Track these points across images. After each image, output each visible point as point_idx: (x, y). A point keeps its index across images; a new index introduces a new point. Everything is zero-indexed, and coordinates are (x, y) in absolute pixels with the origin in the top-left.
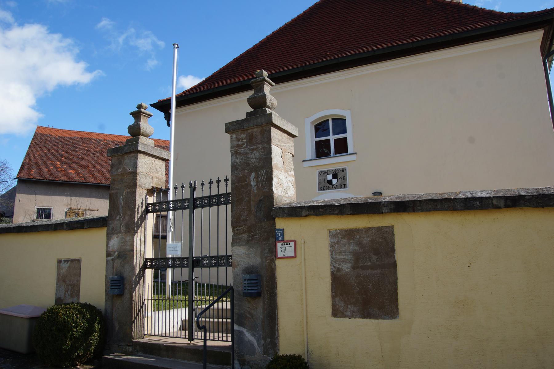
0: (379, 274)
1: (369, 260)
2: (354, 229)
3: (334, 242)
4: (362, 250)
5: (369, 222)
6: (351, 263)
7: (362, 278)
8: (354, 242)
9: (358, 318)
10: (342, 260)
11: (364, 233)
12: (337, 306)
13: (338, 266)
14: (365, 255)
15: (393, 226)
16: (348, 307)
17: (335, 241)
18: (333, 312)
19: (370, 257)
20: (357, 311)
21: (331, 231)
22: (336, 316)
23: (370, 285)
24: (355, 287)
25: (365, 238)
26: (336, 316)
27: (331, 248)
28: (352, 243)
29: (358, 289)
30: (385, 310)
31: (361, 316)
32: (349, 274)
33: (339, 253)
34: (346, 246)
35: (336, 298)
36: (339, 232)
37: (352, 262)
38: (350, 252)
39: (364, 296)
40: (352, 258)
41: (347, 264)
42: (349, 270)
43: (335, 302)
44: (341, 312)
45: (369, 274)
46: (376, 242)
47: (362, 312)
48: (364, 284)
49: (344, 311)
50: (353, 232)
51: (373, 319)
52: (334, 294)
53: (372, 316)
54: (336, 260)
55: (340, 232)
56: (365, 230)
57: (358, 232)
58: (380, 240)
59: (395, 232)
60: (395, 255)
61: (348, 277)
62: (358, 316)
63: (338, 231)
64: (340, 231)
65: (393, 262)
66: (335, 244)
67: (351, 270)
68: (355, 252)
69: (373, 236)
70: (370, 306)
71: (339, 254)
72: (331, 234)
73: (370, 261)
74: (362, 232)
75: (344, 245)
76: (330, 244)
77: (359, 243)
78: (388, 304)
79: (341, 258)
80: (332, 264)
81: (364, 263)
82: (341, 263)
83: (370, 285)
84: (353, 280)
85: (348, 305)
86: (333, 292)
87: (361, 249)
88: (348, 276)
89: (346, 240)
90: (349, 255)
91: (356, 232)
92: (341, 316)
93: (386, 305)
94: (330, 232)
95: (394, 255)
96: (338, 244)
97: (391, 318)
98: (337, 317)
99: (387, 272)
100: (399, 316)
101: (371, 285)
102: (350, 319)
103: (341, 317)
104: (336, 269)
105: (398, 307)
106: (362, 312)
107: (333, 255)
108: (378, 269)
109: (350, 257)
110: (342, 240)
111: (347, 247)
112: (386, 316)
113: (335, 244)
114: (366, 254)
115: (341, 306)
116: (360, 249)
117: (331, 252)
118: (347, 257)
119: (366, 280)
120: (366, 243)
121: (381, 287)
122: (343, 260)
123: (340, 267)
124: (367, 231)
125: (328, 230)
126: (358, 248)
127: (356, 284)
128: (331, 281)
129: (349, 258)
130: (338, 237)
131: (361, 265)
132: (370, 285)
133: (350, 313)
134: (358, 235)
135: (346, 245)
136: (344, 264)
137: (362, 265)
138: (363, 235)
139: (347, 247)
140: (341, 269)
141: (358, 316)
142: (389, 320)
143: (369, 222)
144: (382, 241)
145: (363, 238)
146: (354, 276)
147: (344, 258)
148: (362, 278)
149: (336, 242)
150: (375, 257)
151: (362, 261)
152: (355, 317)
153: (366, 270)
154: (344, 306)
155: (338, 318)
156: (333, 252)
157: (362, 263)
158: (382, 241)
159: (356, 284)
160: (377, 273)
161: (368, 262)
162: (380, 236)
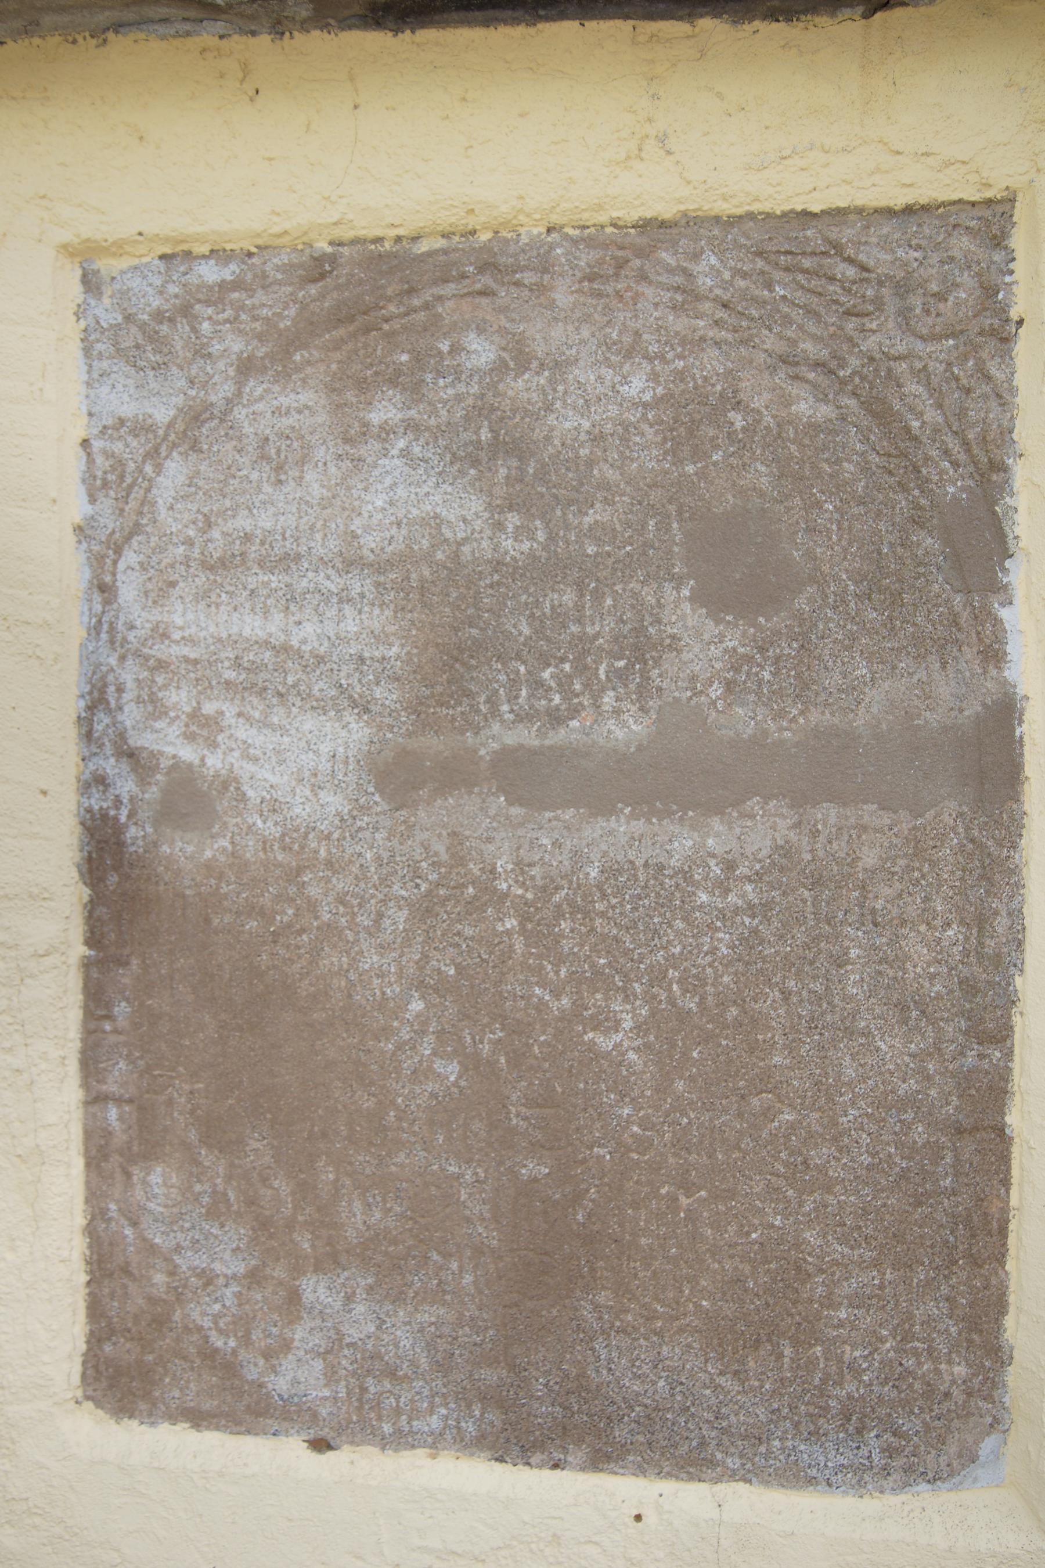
0: (756, 878)
1: (622, 676)
2: (423, 247)
3: (141, 428)
4: (523, 532)
5: (662, 139)
6: (364, 707)
7: (511, 923)
8: (412, 427)
9: (435, 1443)
10: (237, 663)
11: (563, 296)
12: (160, 1278)
13: (188, 753)
14: (569, 598)
15: (1011, 200)
16: (294, 1297)
17: (162, 414)
18: (95, 1340)
19: (639, 630)
20: (424, 1362)
21: (107, 266)
22: (147, 1395)
23: (616, 1027)
24: (405, 1034)
25: (583, 374)
26: (147, 1395)
27: (106, 504)
28: (386, 432)
29: (451, 1070)
30: (813, 1362)
31: (470, 1427)
32: (329, 864)
33: (207, 566)
34: (300, 480)
35: (137, 1172)
36: (223, 286)
37: (385, 695)
38: (351, 563)
39: (533, 1168)
40: (380, 638)
41: (309, 723)
42: (334, 802)
43: (135, 1224)
44: (209, 1354)
45: (610, 871)
46: (738, 420)
47: (489, 1376)
48: (541, 1006)
49: (246, 1340)
50: (411, 291)
51: (640, 1471)
52: (113, 1113)
53: (620, 1433)
54: (162, 665)
55: (237, 285)
56: (585, 258)
57: (486, 280)
58: (804, 407)
59: (1020, 291)
60: (1004, 613)
61: (313, 907)
62: (435, 1422)
63: (210, 273)
64: (229, 272)
65: (973, 709)
66: (152, 455)
67: (365, 809)
68: (428, 557)
69: (696, 343)
70: (604, 1297)
71: (201, 580)
72: (106, 311)
73: (643, 692)
74: (540, 289)
75: (279, 468)
76: (85, 443)
77: (485, 435)
78: (853, 1284)
79: (233, 641)
80: (102, 722)
81: (556, 718)
82: (230, 710)
83: (616, 1027)
84: (383, 948)
85: (297, 1271)
86: (111, 1087)
87: (513, 520)
88: (314, 891)
89: (306, 397)
90: (344, 598)
91: (450, 289)
92: (208, 1405)
93: (830, 1302)
94: (90, 282)
95: (997, 622)
96: (195, 447)
97: (886, 1471)
98: (151, 1418)
99: (869, 858)
100: (997, 1455)
101: (639, 1028)
102: (320, 1445)
103: (198, 1419)
104: (153, 793)
105: (998, 1328)
106: (489, 1376)
107: (128, 592)
108: (754, 803)
109: (351, 626)
110: (254, 387)
111: (317, 491)
112: (815, 1435)
113: (152, 455)
114: (580, 587)
115: (208, 1279)
116: (499, 526)
117: (97, 561)
118: (309, 629)
119: (566, 945)
120: (597, 438)
121: (649, 1093)
122: (254, 669)
123: (214, 762)
124: (621, 265)
125: (67, 250)
126: (475, 505)
127: (417, 1006)
128: (83, 950)
129: (342, 639)
130: (201, 352)
131: (511, 739)
132: (627, 1025)
133: (331, 1375)
134: (481, 331)
135: (302, 462)
136: (264, 724)
137: (526, 736)
138: (557, 332)
139: (317, 491)
140: (228, 783)
141: (435, 1422)
142: (859, 1487)
143: (662, 139)
144: (825, 411)
145: (559, 366)
146: (397, 889)
147: (266, 644)
148: (511, 923)
149: (170, 425)
150: (711, 629)
151: (514, 683)
152: (387, 1428)
153: (568, 814)
154: (254, 1277)
155: (165, 1427)
156: (130, 557)
157: (521, 718)
158: (825, 411)
159: (417, 1006)
160: (730, 866)
161: (608, 699)
162: (807, 346)
